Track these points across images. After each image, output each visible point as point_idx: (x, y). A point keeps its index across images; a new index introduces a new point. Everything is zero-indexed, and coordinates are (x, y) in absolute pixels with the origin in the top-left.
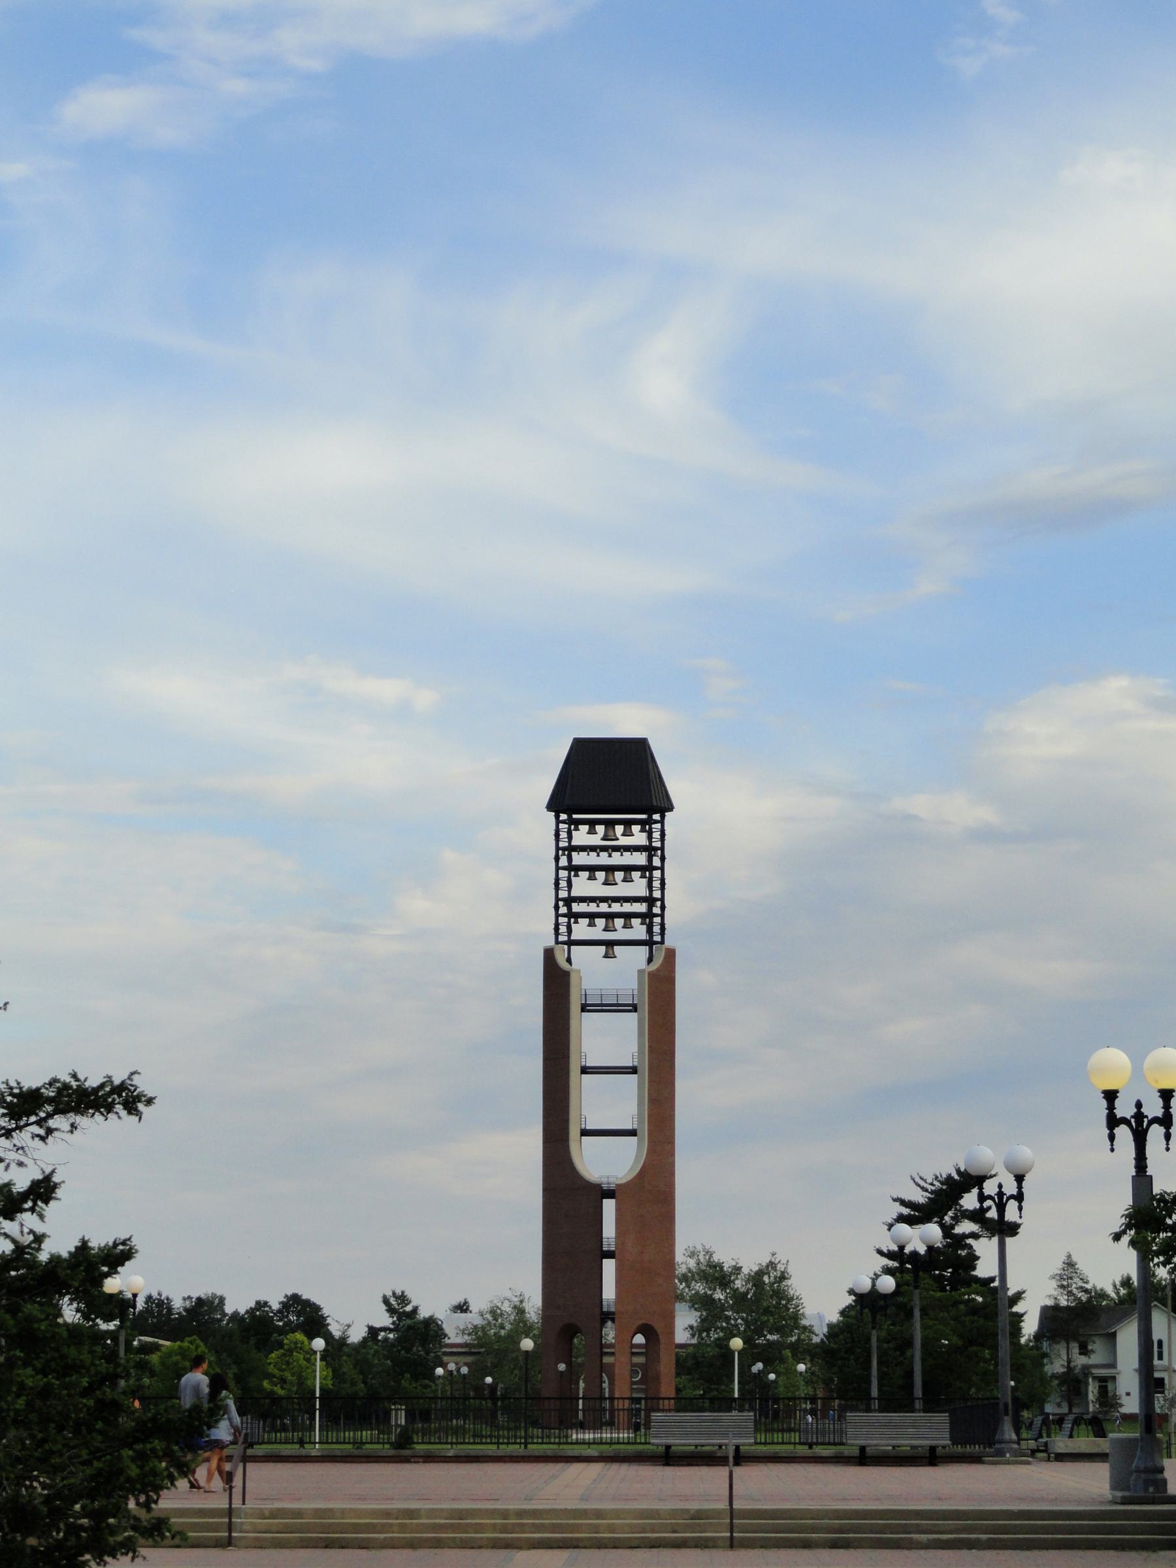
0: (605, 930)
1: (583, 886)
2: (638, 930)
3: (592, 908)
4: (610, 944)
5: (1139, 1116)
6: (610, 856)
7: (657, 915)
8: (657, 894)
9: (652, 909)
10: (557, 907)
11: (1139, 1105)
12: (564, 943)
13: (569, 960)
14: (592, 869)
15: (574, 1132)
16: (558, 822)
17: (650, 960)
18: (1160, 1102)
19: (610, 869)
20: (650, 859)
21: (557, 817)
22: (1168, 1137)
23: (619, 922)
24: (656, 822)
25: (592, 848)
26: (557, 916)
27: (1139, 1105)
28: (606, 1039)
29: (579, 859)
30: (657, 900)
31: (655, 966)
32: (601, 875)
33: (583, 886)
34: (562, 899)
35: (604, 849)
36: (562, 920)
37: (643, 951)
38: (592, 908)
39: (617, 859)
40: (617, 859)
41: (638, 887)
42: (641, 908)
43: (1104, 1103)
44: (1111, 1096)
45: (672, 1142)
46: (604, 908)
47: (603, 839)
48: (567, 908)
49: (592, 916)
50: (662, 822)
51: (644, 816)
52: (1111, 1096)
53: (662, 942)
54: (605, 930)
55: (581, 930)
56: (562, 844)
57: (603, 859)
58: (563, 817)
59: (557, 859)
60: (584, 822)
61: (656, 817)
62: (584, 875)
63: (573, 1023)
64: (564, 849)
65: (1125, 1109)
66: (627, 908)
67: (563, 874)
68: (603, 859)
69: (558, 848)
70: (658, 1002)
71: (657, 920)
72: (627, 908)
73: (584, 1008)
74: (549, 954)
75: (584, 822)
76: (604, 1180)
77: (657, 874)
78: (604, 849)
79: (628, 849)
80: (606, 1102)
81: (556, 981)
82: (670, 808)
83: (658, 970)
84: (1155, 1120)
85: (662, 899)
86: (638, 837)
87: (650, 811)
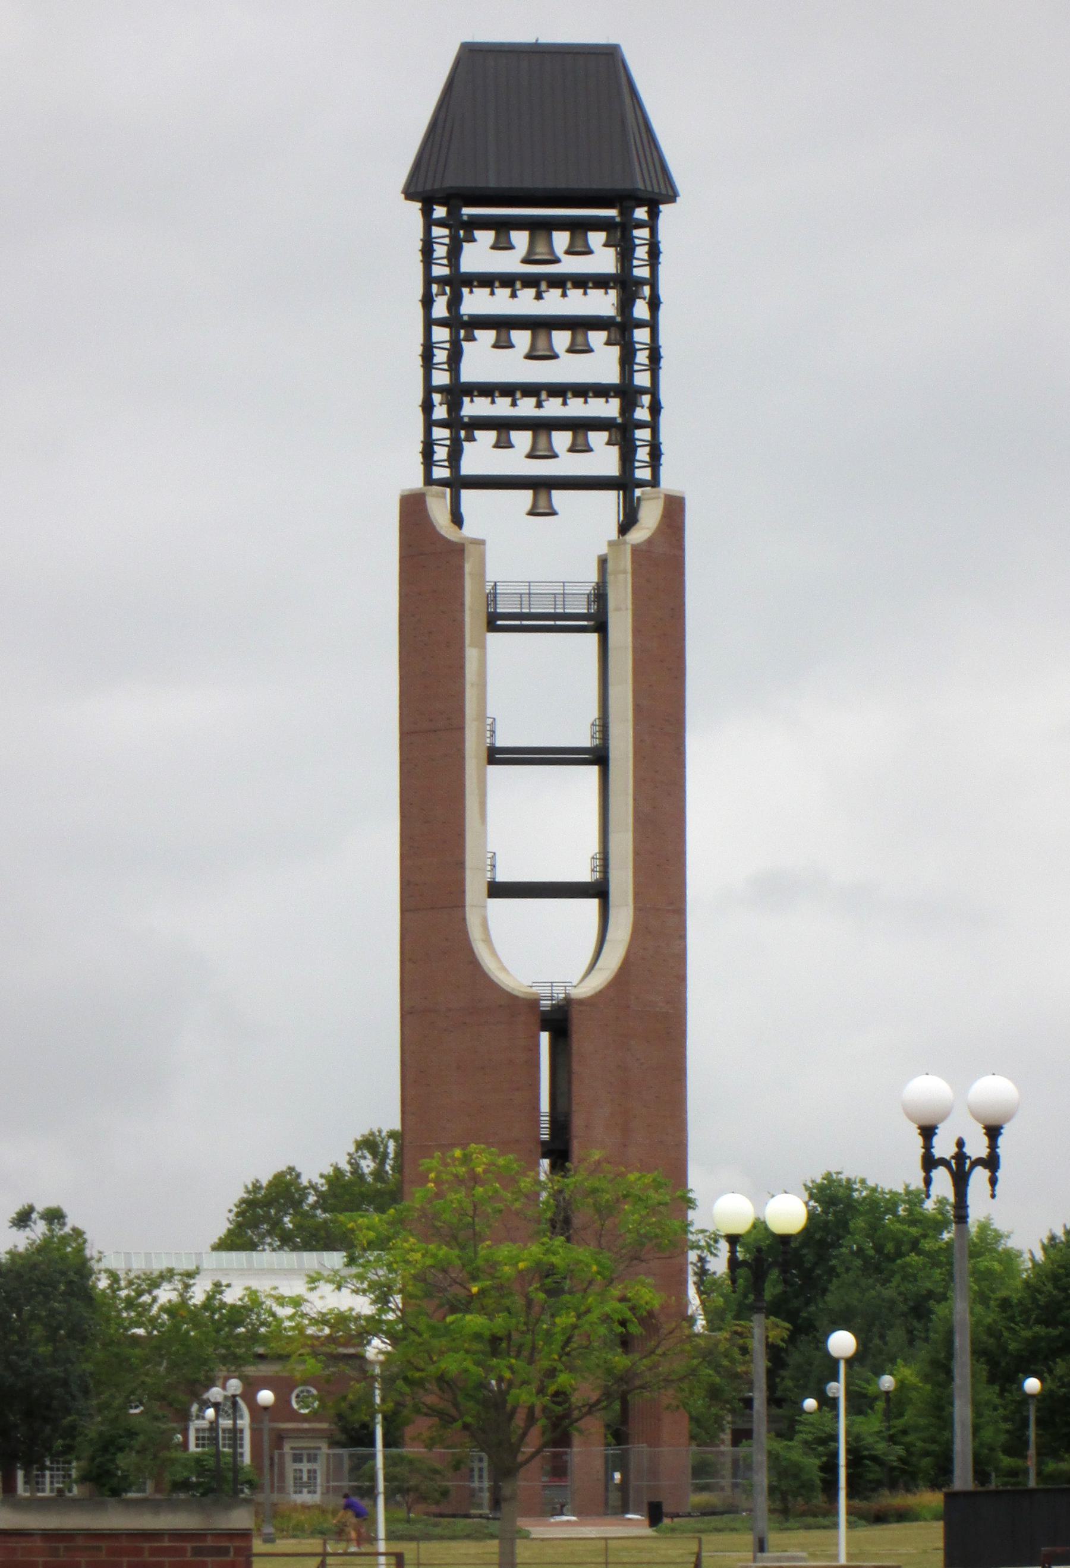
0: (531, 456)
1: (482, 359)
2: (603, 458)
3: (502, 407)
4: (541, 486)
5: (961, 1157)
6: (539, 296)
7: (641, 425)
8: (642, 379)
9: (632, 416)
10: (427, 407)
11: (960, 1144)
12: (443, 483)
13: (457, 519)
14: (503, 325)
15: (475, 887)
16: (429, 223)
17: (627, 524)
18: (985, 1141)
19: (541, 325)
20: (626, 304)
21: (427, 212)
22: (993, 1181)
23: (562, 439)
24: (640, 225)
25: (508, 281)
26: (429, 424)
27: (960, 1144)
28: (535, 687)
29: (477, 302)
30: (643, 391)
31: (638, 535)
32: (522, 338)
33: (482, 359)
34: (440, 389)
35: (531, 281)
36: (439, 433)
37: (609, 501)
38: (502, 407)
39: (554, 303)
40: (554, 303)
41: (602, 363)
42: (610, 408)
43: (920, 1141)
44: (928, 1132)
45: (680, 910)
46: (526, 407)
47: (526, 261)
48: (451, 409)
49: (503, 426)
50: (652, 224)
51: (612, 213)
52: (928, 1132)
53: (655, 482)
54: (531, 456)
55: (481, 455)
56: (438, 271)
57: (525, 303)
58: (440, 212)
59: (427, 302)
60: (485, 223)
61: (641, 213)
62: (486, 337)
63: (471, 654)
64: (442, 281)
65: (944, 1147)
66: (576, 408)
67: (441, 334)
68: (525, 303)
69: (429, 280)
70: (644, 614)
71: (643, 434)
72: (576, 408)
73: (494, 623)
74: (412, 509)
75: (485, 223)
76: (545, 991)
77: (642, 336)
78: (531, 281)
79: (582, 282)
80: (538, 824)
81: (432, 566)
82: (671, 197)
83: (650, 541)
84: (979, 1162)
85: (654, 391)
86: (602, 259)
87: (625, 200)
